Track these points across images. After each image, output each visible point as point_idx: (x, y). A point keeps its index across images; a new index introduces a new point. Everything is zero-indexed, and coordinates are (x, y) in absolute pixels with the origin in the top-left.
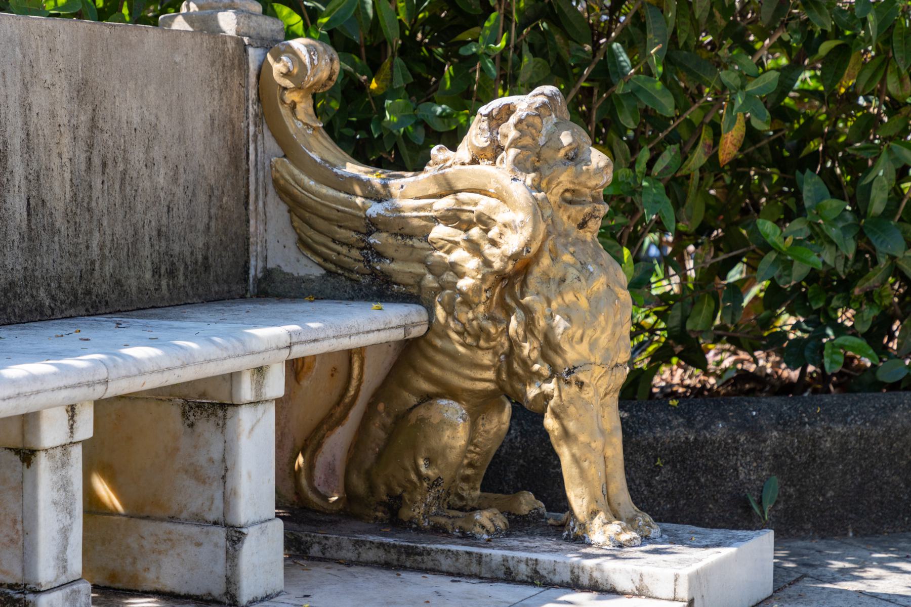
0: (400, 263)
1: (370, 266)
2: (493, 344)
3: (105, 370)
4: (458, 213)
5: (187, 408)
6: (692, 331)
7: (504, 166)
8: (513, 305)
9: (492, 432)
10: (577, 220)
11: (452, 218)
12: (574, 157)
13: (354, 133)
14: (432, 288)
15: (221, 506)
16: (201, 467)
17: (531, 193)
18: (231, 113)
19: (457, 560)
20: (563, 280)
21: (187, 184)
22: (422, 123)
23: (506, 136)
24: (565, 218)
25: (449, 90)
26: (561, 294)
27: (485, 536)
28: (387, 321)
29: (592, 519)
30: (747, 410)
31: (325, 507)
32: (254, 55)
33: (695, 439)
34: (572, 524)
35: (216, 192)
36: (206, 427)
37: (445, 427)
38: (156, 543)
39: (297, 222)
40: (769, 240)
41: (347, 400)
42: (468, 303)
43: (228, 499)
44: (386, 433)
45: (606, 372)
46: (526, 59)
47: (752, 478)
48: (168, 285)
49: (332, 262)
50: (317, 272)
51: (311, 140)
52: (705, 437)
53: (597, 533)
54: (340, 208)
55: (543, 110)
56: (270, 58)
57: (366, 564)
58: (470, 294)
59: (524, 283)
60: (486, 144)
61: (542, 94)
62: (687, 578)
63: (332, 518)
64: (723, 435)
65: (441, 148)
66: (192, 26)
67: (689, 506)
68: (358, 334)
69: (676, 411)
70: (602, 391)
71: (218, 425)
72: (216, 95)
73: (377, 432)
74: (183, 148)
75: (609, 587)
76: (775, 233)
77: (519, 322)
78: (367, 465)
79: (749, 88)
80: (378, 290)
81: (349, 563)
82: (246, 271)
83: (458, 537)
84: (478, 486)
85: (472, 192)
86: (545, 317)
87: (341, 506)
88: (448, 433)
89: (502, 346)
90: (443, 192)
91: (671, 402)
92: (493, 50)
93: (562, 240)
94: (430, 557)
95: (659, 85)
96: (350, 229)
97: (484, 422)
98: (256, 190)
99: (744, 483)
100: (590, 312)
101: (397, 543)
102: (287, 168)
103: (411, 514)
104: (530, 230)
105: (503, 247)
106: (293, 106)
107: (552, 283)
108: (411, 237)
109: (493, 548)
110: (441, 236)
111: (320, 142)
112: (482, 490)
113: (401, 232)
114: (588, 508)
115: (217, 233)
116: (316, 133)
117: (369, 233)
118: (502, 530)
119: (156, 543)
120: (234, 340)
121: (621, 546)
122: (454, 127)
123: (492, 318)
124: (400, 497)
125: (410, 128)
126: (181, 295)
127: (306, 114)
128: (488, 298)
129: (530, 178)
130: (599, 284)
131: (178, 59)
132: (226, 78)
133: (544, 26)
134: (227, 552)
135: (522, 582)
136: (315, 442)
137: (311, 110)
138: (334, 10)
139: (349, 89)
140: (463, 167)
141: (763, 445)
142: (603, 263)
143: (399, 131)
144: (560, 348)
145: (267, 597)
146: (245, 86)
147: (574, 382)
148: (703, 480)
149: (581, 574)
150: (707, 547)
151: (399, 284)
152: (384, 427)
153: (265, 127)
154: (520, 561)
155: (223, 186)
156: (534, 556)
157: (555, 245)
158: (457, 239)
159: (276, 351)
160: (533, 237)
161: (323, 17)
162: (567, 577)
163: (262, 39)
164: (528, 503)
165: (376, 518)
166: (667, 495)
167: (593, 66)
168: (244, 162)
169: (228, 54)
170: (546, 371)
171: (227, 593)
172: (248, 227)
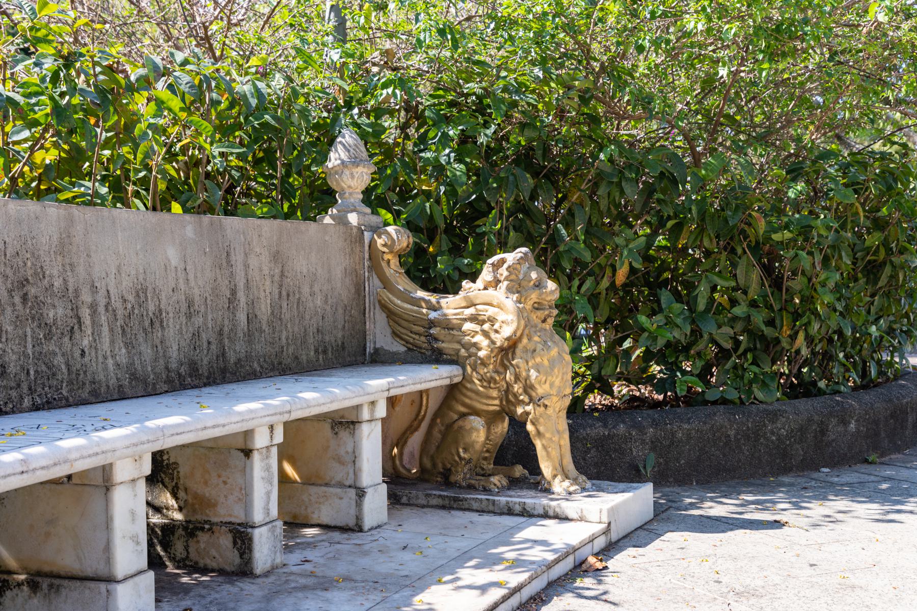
11: (473, 319)
12: (539, 285)
20: (534, 350)
26: (533, 358)
32: (367, 235)
36: (344, 434)
42: (484, 364)
43: (357, 473)
46: (511, 234)
51: (399, 280)
57: (432, 507)
59: (514, 353)
69: (598, 419)
70: (557, 409)
73: (437, 435)
78: (432, 452)
81: (423, 507)
82: (365, 350)
88: (475, 434)
93: (533, 329)
95: (582, 246)
106: (388, 261)
108: (452, 329)
112: (494, 465)
117: (430, 328)
121: (570, 493)
123: (497, 372)
124: (450, 470)
129: (515, 297)
130: (554, 352)
131: (327, 238)
139: (418, 252)
152: (440, 431)
154: (515, 503)
156: (523, 500)
160: (518, 328)
162: (541, 512)
170: (527, 400)
171: (357, 525)
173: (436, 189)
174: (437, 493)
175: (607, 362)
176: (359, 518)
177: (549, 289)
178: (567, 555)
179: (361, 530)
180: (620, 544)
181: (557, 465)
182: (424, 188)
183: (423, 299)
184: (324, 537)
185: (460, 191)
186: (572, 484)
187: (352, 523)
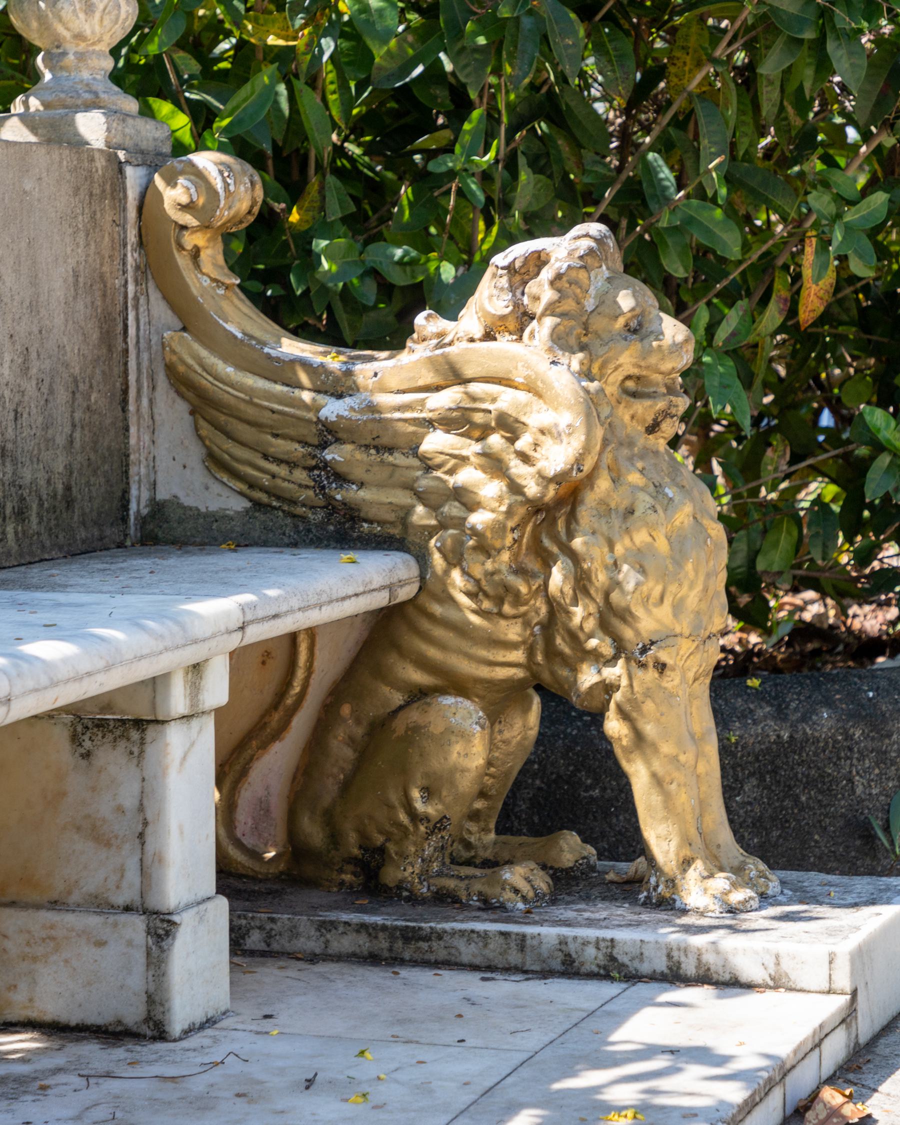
0: (374, 489)
1: (324, 494)
2: (523, 609)
3: (6, 683)
4: (468, 412)
5: (79, 728)
6: (765, 572)
7: (536, 342)
8: (555, 549)
9: (514, 741)
10: (645, 420)
11: (458, 421)
12: (637, 329)
13: (261, 287)
14: (425, 527)
15: (137, 880)
16: (104, 820)
17: (579, 382)
18: (102, 265)
19: (486, 945)
20: (631, 512)
21: (41, 376)
22: (373, 273)
23: (536, 298)
24: (627, 418)
25: (408, 223)
26: (628, 531)
27: (521, 906)
28: (367, 580)
29: (685, 871)
30: (859, 689)
31: (257, 869)
32: (133, 176)
33: (791, 737)
34: (653, 880)
35: (81, 387)
36: (111, 757)
37: (453, 738)
38: (28, 944)
39: (206, 430)
40: (880, 436)
41: (289, 701)
42: (484, 549)
43: (149, 870)
44: (355, 751)
45: (697, 647)
46: (523, 177)
47: (874, 792)
48: (16, 533)
49: (263, 489)
50: (238, 504)
51: (225, 305)
52: (805, 733)
53: (693, 893)
54: (276, 407)
55: (589, 260)
56: (158, 180)
57: (338, 958)
58: (489, 534)
59: (572, 517)
60: (507, 311)
61: (587, 235)
62: (848, 957)
63: (269, 886)
64: (830, 729)
65: (429, 316)
66: (36, 134)
67: (785, 839)
68: (330, 602)
69: (759, 695)
70: (691, 675)
71: (131, 753)
72: (81, 238)
73: (341, 749)
74: (36, 322)
75: (727, 977)
76: (888, 426)
77: (566, 577)
78: (326, 800)
79: (848, 218)
80: (337, 531)
81: (313, 959)
82: (125, 507)
83: (479, 909)
84: (492, 825)
85: (493, 383)
86: (606, 567)
87: (282, 866)
88: (457, 748)
89: (537, 612)
90: (442, 383)
91: (749, 683)
92: (477, 165)
93: (625, 452)
94: (442, 943)
95: (718, 213)
96: (292, 439)
97: (501, 727)
98: (138, 380)
99: (863, 801)
100: (672, 558)
101: (389, 923)
102: (189, 348)
103: (400, 875)
104: (583, 438)
105: (540, 465)
106: (196, 253)
107: (613, 516)
108: (390, 450)
109: (540, 923)
110: (440, 448)
111: (236, 306)
112: (498, 832)
113: (376, 442)
114: (677, 854)
115: (83, 448)
116: (229, 294)
117: (324, 446)
118: (544, 895)
119: (28, 944)
120: (170, 623)
121: (732, 910)
122: (420, 278)
123: (520, 571)
124: (382, 850)
125: (355, 281)
126: (34, 548)
127: (215, 265)
128: (515, 541)
129: (576, 360)
130: (683, 515)
131: (28, 187)
132: (95, 213)
133: (542, 127)
134: (149, 954)
135: (591, 976)
136: (238, 767)
137: (221, 259)
138: (237, 107)
139: (266, 222)
140: (472, 345)
141: (887, 741)
142: (685, 483)
143: (336, 285)
144: (631, 613)
145: (208, 1021)
146: (122, 225)
147: (651, 664)
148: (803, 799)
149: (683, 959)
150: (855, 905)
151: (371, 522)
152: (351, 741)
153: (151, 285)
154: (586, 943)
155: (91, 378)
156: (608, 934)
157: (615, 459)
158: (464, 453)
159: (226, 636)
160: (586, 449)
161: (223, 119)
162: (661, 965)
163: (142, 152)
164: (572, 850)
165: (342, 883)
166: (754, 824)
167: (618, 186)
168: (120, 339)
169: (96, 177)
170: (608, 650)
171: (148, 1019)
172: (128, 437)
173: (309, 45)
174: (354, 918)
175: (771, 537)
176: (155, 1001)
177: (667, 340)
178: (770, 1085)
179: (160, 1034)
180: (882, 1048)
181: (693, 831)
182: (272, 40)
183: (306, 364)
184: (59, 1060)
185: (379, 53)
186: (734, 885)
187: (132, 1013)
